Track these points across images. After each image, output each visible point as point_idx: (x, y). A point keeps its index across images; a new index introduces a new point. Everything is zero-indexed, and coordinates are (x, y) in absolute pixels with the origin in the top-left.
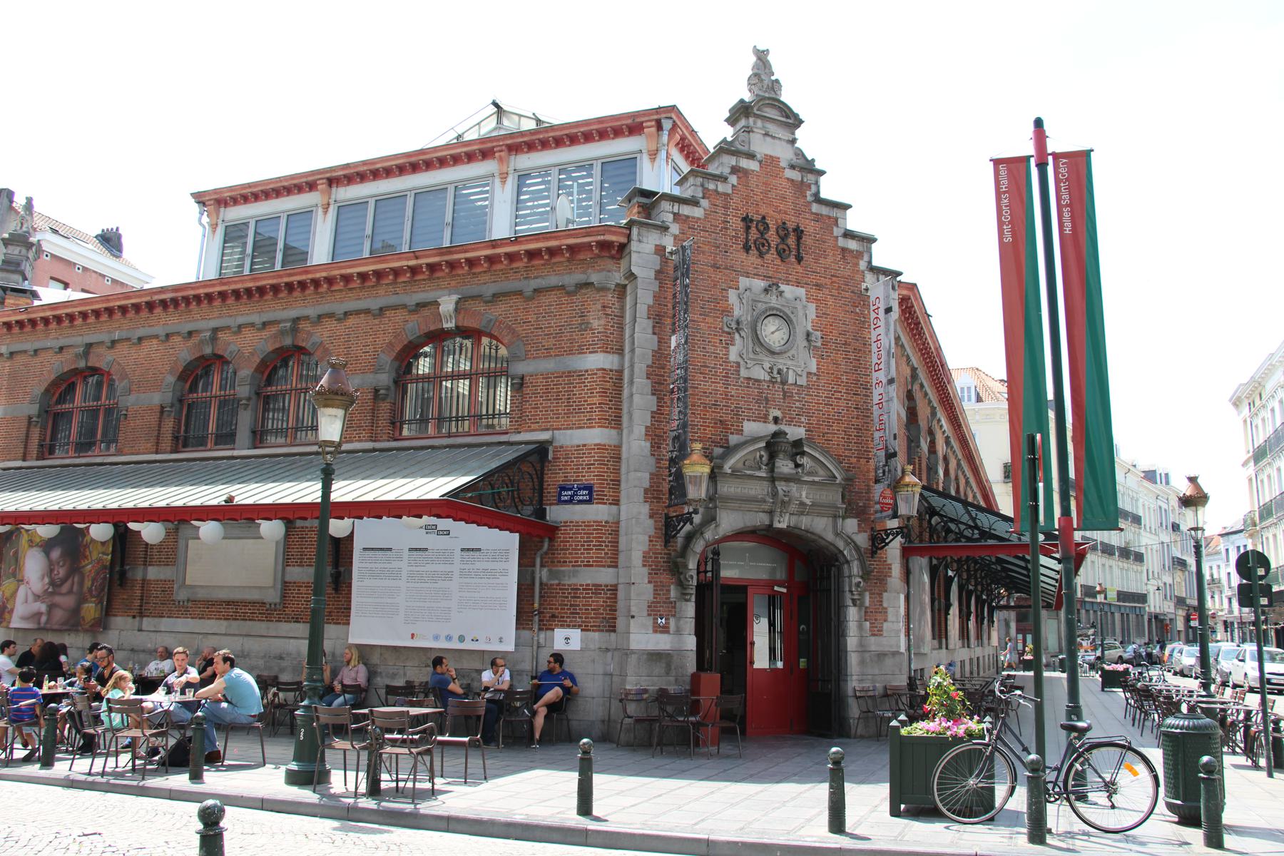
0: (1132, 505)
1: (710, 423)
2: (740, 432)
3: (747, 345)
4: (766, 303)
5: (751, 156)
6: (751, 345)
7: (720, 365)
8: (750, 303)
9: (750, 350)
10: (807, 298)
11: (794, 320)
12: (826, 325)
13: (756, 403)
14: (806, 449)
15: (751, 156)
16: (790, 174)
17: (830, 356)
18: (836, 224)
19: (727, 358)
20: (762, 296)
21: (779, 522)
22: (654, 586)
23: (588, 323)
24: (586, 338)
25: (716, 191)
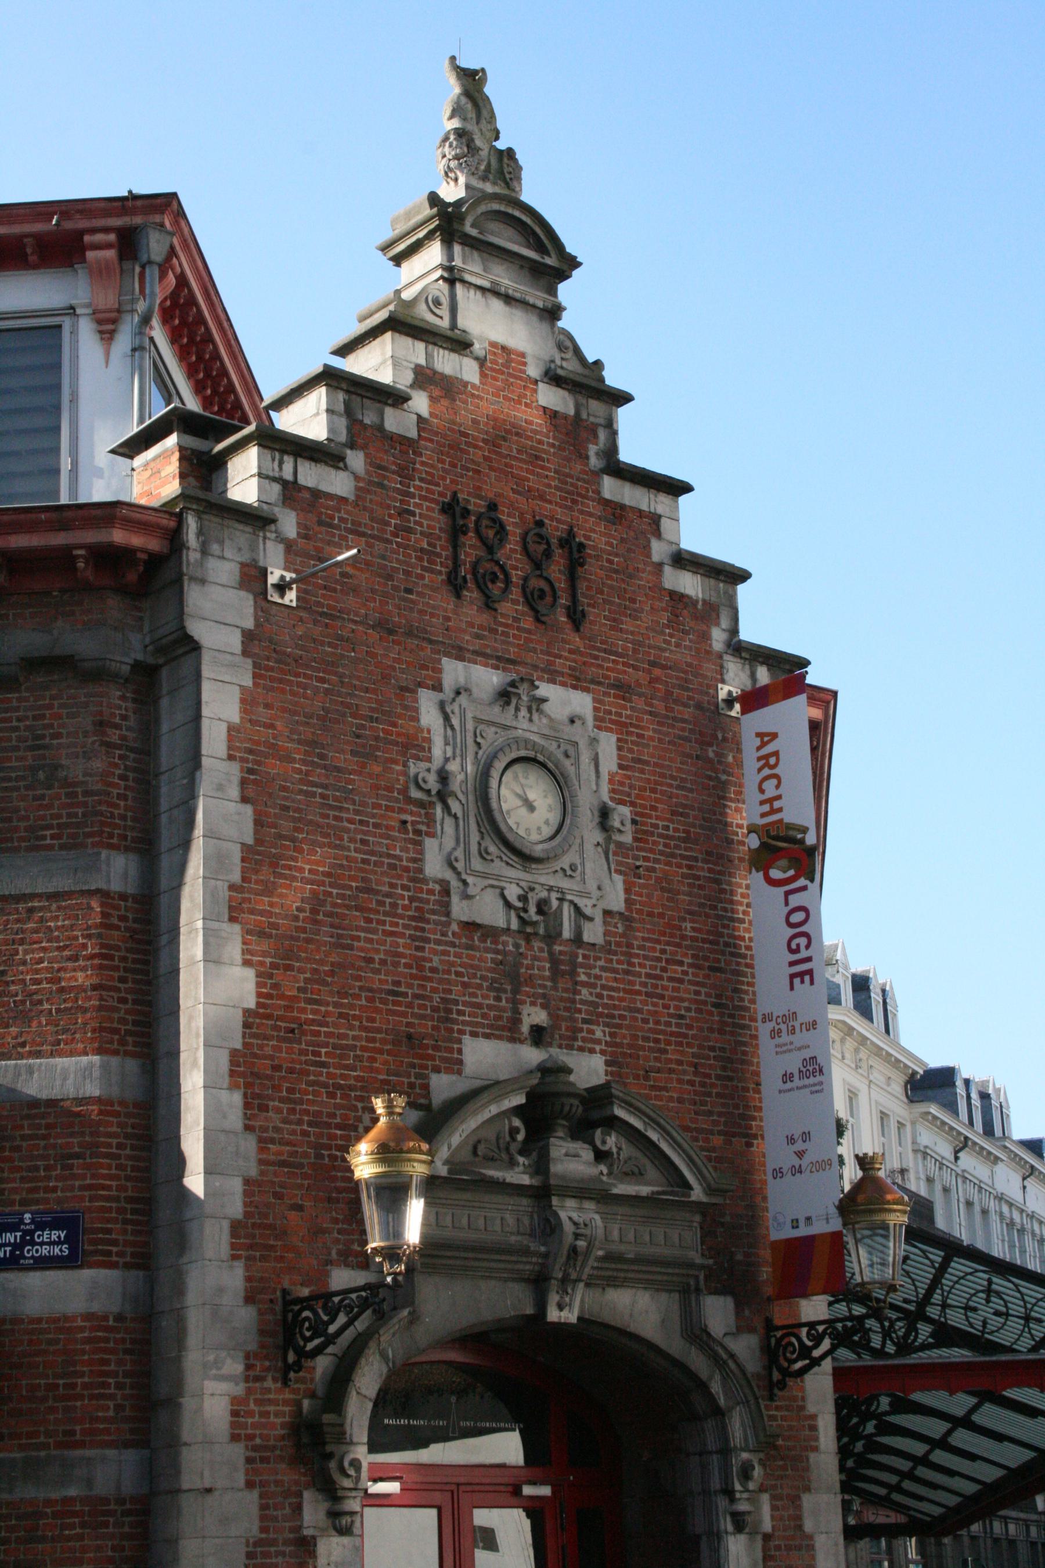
0: (1012, 1246)
1: (383, 1041)
2: (455, 1065)
3: (467, 836)
4: (506, 728)
5: (460, 344)
6: (475, 837)
7: (404, 887)
8: (470, 725)
9: (474, 848)
10: (596, 718)
11: (571, 770)
12: (642, 789)
13: (489, 989)
14: (619, 1112)
15: (460, 344)
16: (549, 397)
17: (654, 870)
18: (658, 534)
19: (421, 871)
20: (497, 709)
21: (561, 1307)
22: (261, 1496)
23: (56, 767)
24: (50, 806)
25: (380, 428)
